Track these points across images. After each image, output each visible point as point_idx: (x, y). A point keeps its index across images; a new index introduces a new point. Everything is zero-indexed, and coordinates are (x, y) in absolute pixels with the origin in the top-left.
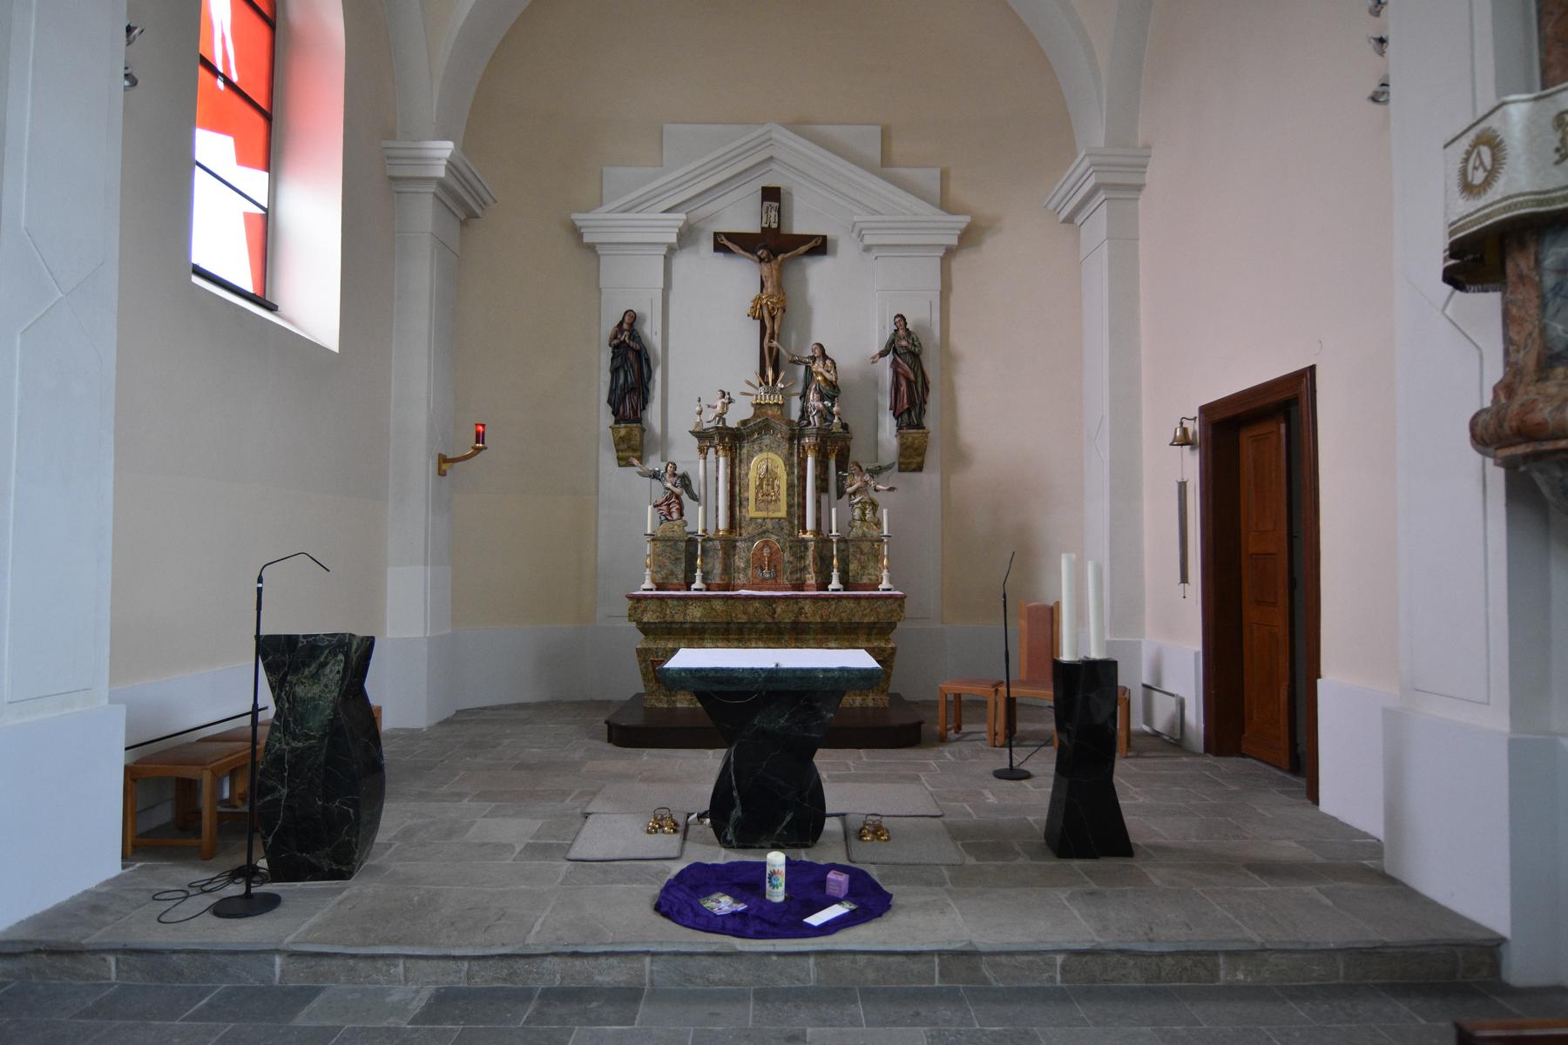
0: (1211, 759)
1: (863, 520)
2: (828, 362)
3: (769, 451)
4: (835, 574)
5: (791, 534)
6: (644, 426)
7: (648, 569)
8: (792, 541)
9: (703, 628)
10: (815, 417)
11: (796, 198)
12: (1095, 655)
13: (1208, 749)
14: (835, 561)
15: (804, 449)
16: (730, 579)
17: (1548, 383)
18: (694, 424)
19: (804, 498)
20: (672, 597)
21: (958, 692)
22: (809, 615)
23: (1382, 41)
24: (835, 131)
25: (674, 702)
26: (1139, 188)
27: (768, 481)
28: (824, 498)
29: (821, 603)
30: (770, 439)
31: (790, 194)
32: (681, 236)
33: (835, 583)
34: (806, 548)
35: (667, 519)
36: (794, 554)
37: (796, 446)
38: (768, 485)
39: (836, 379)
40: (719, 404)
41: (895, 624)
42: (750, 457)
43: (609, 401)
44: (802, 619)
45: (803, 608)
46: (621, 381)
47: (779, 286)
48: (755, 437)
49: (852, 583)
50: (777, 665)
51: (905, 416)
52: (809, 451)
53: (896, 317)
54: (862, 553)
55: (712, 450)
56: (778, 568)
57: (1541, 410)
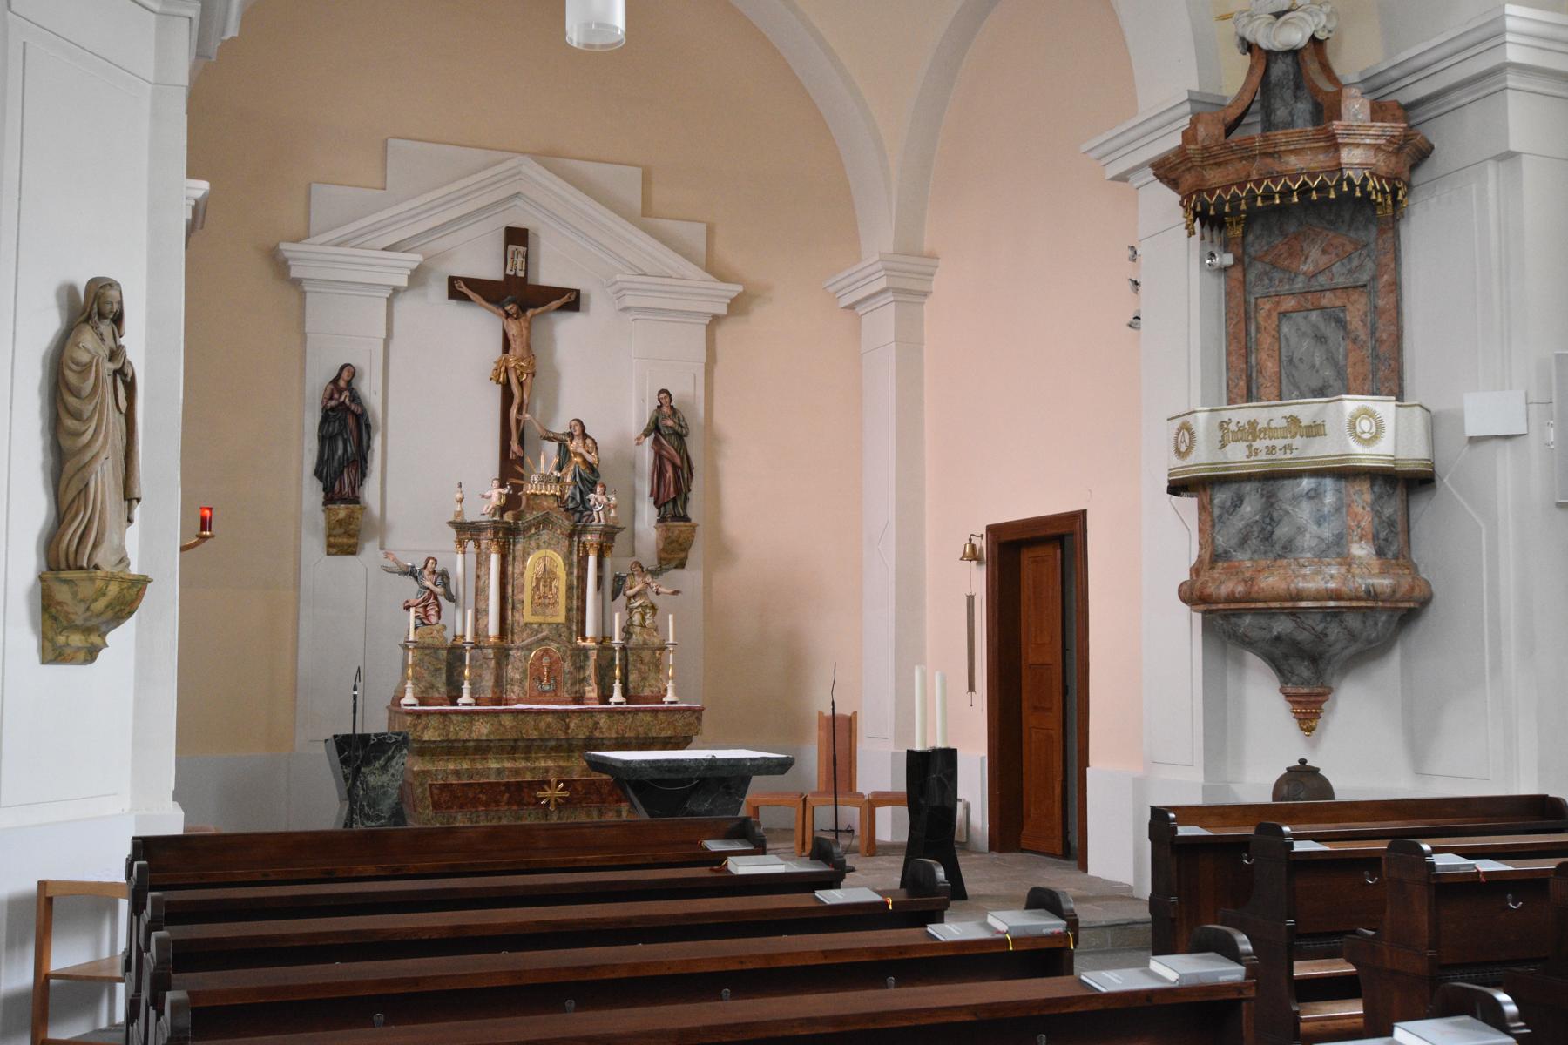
0: (995, 855)
1: (643, 626)
3: (547, 548)
4: (617, 686)
8: (573, 649)
12: (940, 745)
13: (992, 847)
15: (585, 547)
16: (501, 692)
17: (1215, 571)
22: (604, 730)
23: (1136, 283)
24: (590, 169)
26: (925, 294)
29: (616, 717)
30: (548, 534)
31: (537, 236)
33: (617, 697)
34: (587, 657)
35: (423, 623)
36: (574, 664)
41: (691, 738)
42: (526, 554)
43: (318, 473)
44: (597, 734)
45: (598, 723)
48: (533, 531)
51: (670, 506)
54: (642, 662)
57: (1210, 587)
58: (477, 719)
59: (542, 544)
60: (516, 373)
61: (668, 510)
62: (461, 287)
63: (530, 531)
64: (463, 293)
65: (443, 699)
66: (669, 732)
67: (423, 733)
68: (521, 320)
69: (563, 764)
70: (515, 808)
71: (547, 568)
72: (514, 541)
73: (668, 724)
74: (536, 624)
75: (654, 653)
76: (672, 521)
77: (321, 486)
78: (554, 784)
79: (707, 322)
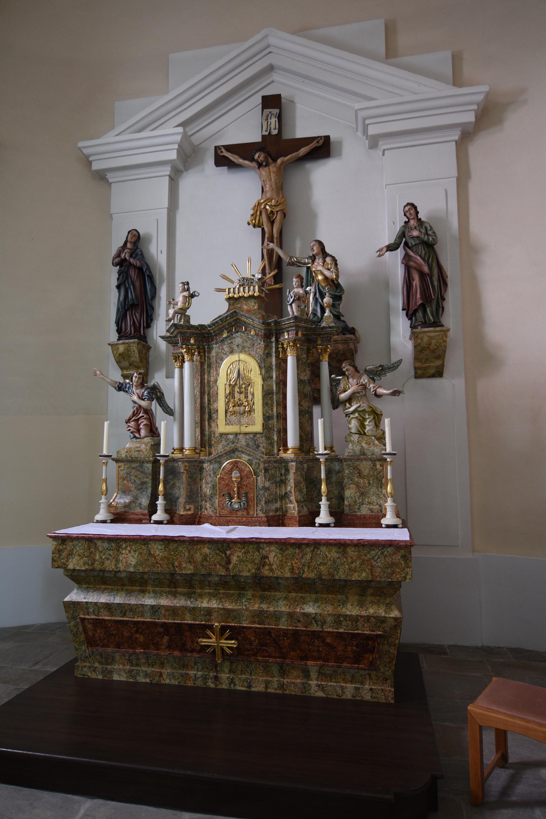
1: (361, 433)
2: (328, 260)
3: (241, 352)
4: (324, 504)
9: (142, 578)
10: (293, 305)
11: (298, 106)
15: (283, 344)
21: (502, 727)
24: (334, 31)
25: (111, 672)
27: (240, 388)
29: (290, 551)
33: (324, 517)
34: (287, 470)
35: (135, 437)
36: (271, 478)
37: (274, 345)
38: (241, 393)
41: (399, 583)
44: (266, 572)
45: (267, 557)
48: (225, 336)
51: (420, 314)
54: (360, 475)
56: (251, 495)
58: (124, 546)
59: (235, 348)
61: (418, 318)
62: (222, 152)
63: (222, 335)
67: (67, 561)
68: (270, 167)
69: (229, 606)
70: (177, 653)
71: (241, 372)
73: (363, 563)
74: (231, 434)
75: (375, 465)
76: (421, 328)
77: (147, 339)
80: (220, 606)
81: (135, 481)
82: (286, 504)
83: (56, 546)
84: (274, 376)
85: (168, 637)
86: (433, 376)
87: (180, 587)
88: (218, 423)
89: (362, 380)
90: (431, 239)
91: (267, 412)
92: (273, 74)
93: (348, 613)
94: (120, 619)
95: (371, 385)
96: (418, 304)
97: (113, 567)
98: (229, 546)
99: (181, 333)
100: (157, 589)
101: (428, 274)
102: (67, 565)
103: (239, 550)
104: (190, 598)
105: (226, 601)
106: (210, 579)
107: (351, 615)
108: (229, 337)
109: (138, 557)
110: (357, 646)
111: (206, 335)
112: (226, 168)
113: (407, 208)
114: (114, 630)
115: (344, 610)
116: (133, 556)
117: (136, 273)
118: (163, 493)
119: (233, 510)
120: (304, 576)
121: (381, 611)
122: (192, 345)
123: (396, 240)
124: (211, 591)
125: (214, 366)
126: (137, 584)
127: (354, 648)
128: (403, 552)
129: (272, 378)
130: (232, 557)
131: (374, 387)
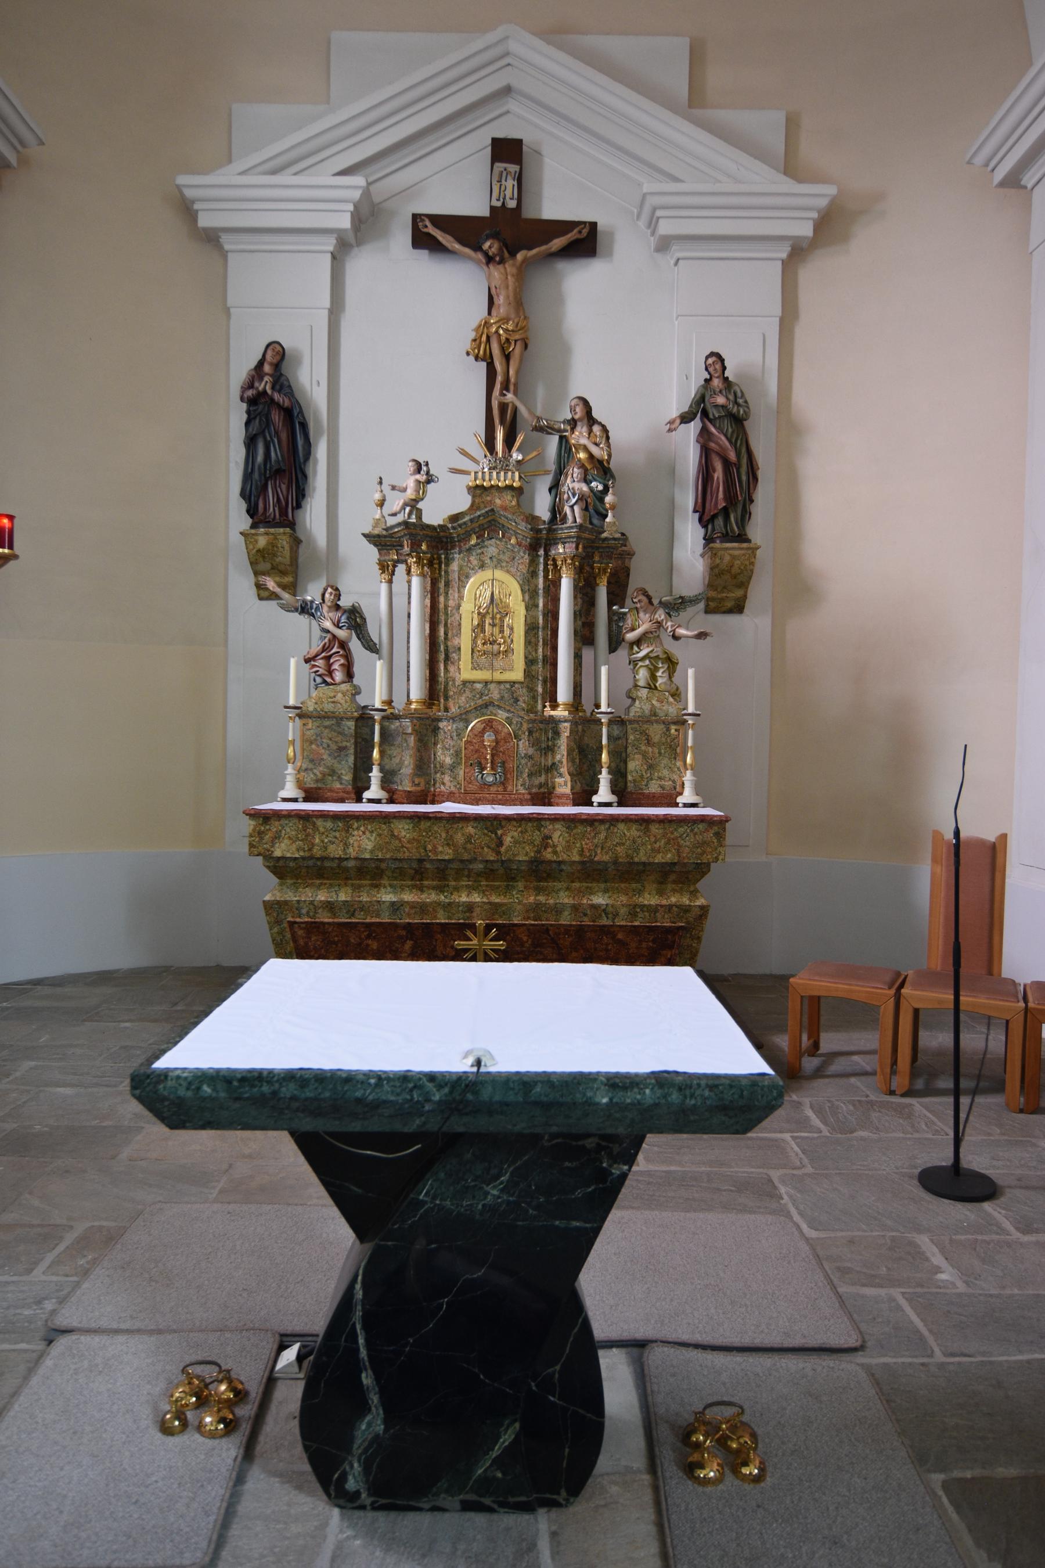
1: (652, 687)
2: (596, 429)
3: (496, 567)
4: (604, 779)
5: (531, 710)
6: (300, 534)
7: (290, 766)
8: (533, 721)
9: (377, 868)
10: (576, 508)
11: (547, 161)
14: (604, 756)
15: (555, 565)
16: (428, 783)
18: (372, 522)
19: (555, 649)
20: (323, 815)
24: (614, 45)
27: (493, 618)
28: (587, 654)
29: (580, 829)
32: (360, 221)
33: (604, 793)
34: (557, 734)
35: (325, 682)
36: (535, 743)
37: (542, 560)
39: (610, 455)
40: (411, 483)
41: (708, 865)
42: (464, 577)
43: (243, 494)
44: (548, 855)
45: (551, 838)
46: (260, 458)
47: (519, 303)
48: (473, 542)
49: (631, 793)
50: (478, 1063)
51: (720, 522)
52: (564, 568)
53: (707, 358)
54: (649, 742)
55: (401, 569)
56: (509, 765)
58: (356, 825)
59: (488, 561)
60: (499, 340)
61: (717, 527)
62: (426, 227)
63: (469, 540)
64: (429, 234)
65: (348, 793)
66: (669, 856)
67: (272, 846)
69: (495, 899)
72: (447, 558)
73: (668, 843)
75: (668, 730)
76: (721, 542)
78: (481, 930)
79: (784, 255)
80: (485, 900)
81: (328, 746)
82: (553, 777)
83: (255, 826)
84: (541, 605)
85: (412, 942)
86: (730, 611)
87: (427, 879)
88: (461, 667)
89: (657, 616)
90: (742, 412)
91: (530, 653)
92: (510, 100)
93: (646, 902)
94: (346, 920)
95: (669, 624)
96: (720, 507)
97: (340, 853)
98: (500, 824)
99: (411, 535)
100: (395, 882)
101: (735, 464)
102: (273, 852)
103: (515, 829)
104: (442, 892)
105: (491, 895)
106: (471, 867)
107: (650, 905)
108: (479, 544)
109: (375, 839)
110: (654, 941)
111: (445, 540)
112: (426, 252)
113: (710, 361)
114: (337, 936)
115: (641, 899)
116: (368, 838)
117: (282, 417)
118: (378, 762)
119: (485, 784)
120: (596, 859)
121: (684, 900)
122: (424, 553)
123: (691, 406)
124: (470, 883)
125: (456, 585)
126: (368, 877)
127: (651, 944)
128: (716, 828)
129: (537, 606)
130: (504, 837)
131: (672, 626)
